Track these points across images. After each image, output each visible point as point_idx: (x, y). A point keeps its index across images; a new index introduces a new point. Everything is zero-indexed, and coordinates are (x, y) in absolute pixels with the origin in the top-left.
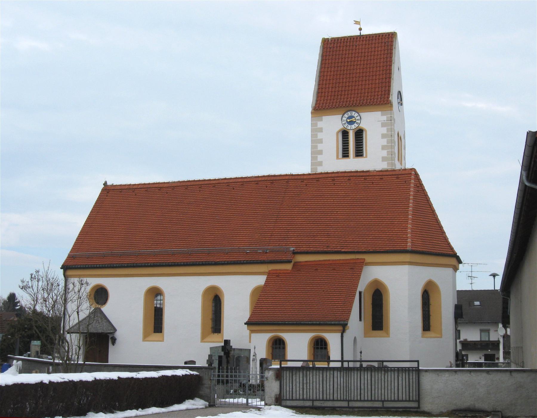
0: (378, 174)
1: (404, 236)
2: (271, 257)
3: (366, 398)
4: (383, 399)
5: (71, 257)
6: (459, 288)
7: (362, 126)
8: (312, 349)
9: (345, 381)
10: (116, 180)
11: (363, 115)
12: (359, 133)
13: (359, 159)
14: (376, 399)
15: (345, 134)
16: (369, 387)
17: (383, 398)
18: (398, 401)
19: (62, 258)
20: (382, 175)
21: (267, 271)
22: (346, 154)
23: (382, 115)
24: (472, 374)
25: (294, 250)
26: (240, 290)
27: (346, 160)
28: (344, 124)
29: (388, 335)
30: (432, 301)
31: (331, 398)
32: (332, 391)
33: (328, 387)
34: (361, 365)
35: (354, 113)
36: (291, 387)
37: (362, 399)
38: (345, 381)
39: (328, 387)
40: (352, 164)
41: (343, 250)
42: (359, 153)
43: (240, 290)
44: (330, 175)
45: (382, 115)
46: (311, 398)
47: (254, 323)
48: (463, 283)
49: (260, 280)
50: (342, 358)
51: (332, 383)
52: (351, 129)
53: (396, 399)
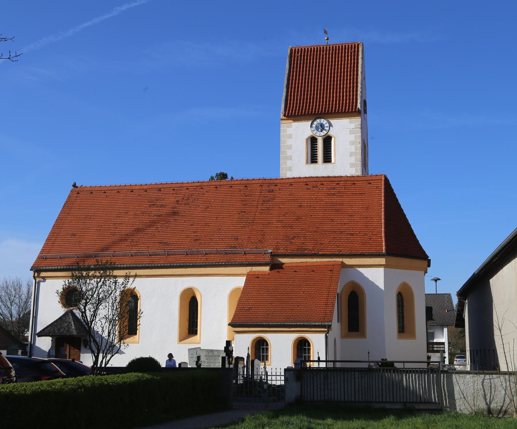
0: (349, 179)
1: (379, 240)
2: (251, 258)
3: (388, 400)
4: (405, 401)
5: (41, 258)
6: (427, 292)
7: (331, 133)
8: (296, 349)
9: (366, 381)
10: (86, 181)
11: (333, 121)
12: (327, 140)
13: (328, 165)
14: (398, 400)
15: (313, 140)
16: (391, 388)
17: (405, 399)
18: (393, 402)
19: (32, 259)
20: (351, 181)
21: (246, 273)
22: (313, 160)
23: (350, 123)
24: (461, 375)
25: (271, 252)
26: (219, 291)
27: (313, 165)
28: (313, 131)
29: (363, 335)
30: (405, 304)
31: (392, 400)
32: (353, 392)
33: (350, 388)
34: (369, 366)
35: (322, 120)
36: (312, 388)
37: (384, 400)
38: (366, 381)
39: (350, 388)
40: (320, 170)
41: (320, 253)
42: (327, 159)
43: (219, 291)
44: (302, 180)
45: (350, 123)
46: (369, 400)
47: (237, 323)
48: (430, 288)
49: (240, 282)
50: (326, 358)
51: (353, 384)
52: (320, 136)
53: (381, 400)
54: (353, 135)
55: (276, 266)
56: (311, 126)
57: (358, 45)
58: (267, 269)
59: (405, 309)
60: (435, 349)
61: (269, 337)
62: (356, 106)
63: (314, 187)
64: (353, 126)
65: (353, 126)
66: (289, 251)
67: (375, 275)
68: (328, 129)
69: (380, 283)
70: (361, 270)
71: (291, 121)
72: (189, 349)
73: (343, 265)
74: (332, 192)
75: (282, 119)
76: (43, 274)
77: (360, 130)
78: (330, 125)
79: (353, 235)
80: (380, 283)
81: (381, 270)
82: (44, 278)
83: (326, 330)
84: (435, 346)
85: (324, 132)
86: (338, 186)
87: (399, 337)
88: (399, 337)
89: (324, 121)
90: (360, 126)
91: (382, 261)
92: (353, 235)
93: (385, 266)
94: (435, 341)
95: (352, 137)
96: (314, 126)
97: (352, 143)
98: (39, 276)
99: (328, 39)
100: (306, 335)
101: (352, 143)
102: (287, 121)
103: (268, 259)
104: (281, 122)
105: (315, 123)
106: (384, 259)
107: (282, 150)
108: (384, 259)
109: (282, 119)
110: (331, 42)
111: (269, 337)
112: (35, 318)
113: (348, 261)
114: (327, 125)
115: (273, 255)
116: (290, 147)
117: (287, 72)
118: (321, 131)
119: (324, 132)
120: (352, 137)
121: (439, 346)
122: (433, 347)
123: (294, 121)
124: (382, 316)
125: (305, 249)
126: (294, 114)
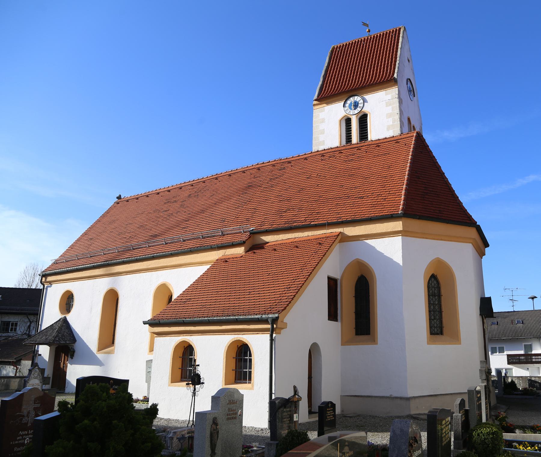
7: (365, 110)
11: (367, 97)
12: (363, 120)
29: (374, 341)
35: (356, 97)
54: (391, 107)
55: (255, 247)
56: (344, 106)
57: (400, 29)
58: (240, 250)
59: (443, 298)
60: (534, 360)
61: (195, 340)
62: (393, 74)
63: (330, 157)
64: (389, 97)
65: (389, 97)
66: (274, 226)
67: (389, 247)
68: (362, 105)
69: (398, 257)
70: (370, 242)
71: (325, 105)
72: (147, 361)
73: (344, 239)
74: (350, 158)
75: (314, 105)
76: (50, 279)
77: (397, 100)
78: (365, 101)
79: (362, 198)
80: (398, 257)
81: (398, 240)
82: (51, 283)
83: (269, 326)
84: (534, 357)
85: (359, 109)
86: (359, 151)
87: (430, 342)
88: (430, 342)
89: (357, 99)
90: (397, 96)
91: (398, 225)
92: (362, 198)
93: (404, 233)
94: (533, 352)
95: (389, 110)
96: (347, 105)
97: (389, 116)
98: (46, 282)
99: (369, 31)
100: (244, 336)
101: (389, 116)
102: (320, 106)
103: (244, 237)
104: (315, 108)
105: (349, 102)
106: (401, 222)
107: (315, 136)
108: (401, 222)
109: (314, 105)
110: (372, 34)
111: (195, 340)
112: (41, 325)
113: (350, 231)
114: (362, 101)
115: (253, 233)
116: (323, 132)
117: (326, 65)
118: (355, 109)
119: (359, 109)
120: (389, 110)
121: (537, 357)
122: (531, 359)
123: (328, 103)
124: (402, 308)
125: (295, 222)
126: (326, 96)
